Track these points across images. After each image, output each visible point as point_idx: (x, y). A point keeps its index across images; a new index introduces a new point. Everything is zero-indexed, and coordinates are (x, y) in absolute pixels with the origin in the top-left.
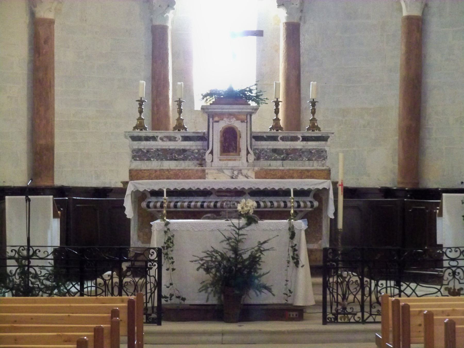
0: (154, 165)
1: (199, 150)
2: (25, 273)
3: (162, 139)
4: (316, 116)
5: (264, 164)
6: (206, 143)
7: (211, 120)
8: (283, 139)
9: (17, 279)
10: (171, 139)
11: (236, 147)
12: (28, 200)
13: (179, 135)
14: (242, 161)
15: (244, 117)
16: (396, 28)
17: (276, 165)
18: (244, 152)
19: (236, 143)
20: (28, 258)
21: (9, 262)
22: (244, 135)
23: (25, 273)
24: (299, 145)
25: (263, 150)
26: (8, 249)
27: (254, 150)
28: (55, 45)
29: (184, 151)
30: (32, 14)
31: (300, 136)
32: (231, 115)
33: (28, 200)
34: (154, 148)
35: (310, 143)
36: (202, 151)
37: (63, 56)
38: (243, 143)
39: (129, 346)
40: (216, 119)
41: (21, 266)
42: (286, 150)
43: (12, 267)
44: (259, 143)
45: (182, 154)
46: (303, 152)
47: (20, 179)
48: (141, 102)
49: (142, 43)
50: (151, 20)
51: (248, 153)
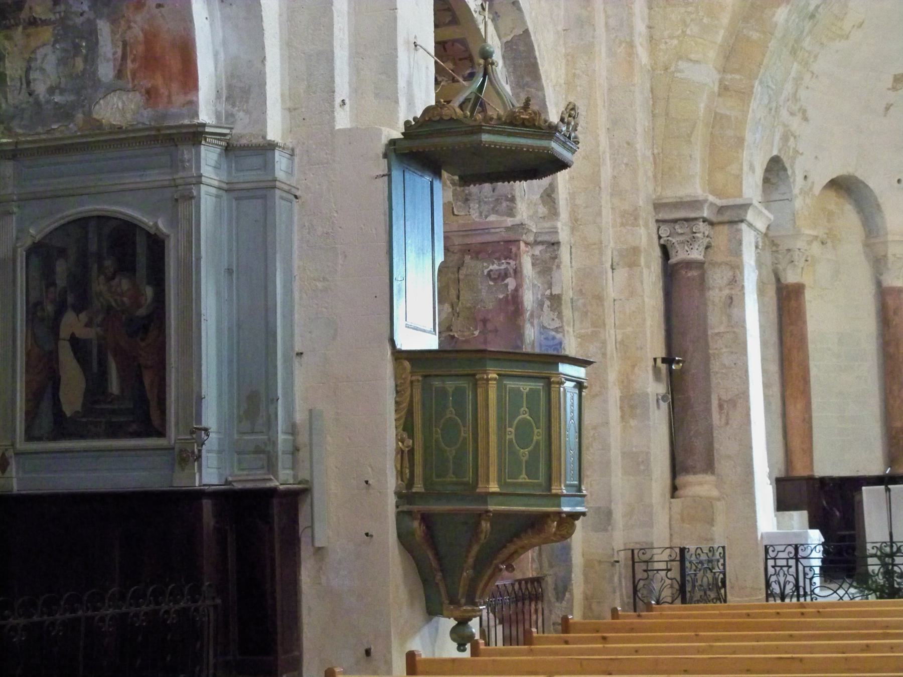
2: (889, 574)
9: (880, 580)
12: (888, 490)
20: (892, 555)
21: (870, 561)
23: (889, 574)
26: (869, 546)
30: (879, 284)
33: (888, 490)
41: (884, 565)
43: (874, 566)
47: (875, 466)
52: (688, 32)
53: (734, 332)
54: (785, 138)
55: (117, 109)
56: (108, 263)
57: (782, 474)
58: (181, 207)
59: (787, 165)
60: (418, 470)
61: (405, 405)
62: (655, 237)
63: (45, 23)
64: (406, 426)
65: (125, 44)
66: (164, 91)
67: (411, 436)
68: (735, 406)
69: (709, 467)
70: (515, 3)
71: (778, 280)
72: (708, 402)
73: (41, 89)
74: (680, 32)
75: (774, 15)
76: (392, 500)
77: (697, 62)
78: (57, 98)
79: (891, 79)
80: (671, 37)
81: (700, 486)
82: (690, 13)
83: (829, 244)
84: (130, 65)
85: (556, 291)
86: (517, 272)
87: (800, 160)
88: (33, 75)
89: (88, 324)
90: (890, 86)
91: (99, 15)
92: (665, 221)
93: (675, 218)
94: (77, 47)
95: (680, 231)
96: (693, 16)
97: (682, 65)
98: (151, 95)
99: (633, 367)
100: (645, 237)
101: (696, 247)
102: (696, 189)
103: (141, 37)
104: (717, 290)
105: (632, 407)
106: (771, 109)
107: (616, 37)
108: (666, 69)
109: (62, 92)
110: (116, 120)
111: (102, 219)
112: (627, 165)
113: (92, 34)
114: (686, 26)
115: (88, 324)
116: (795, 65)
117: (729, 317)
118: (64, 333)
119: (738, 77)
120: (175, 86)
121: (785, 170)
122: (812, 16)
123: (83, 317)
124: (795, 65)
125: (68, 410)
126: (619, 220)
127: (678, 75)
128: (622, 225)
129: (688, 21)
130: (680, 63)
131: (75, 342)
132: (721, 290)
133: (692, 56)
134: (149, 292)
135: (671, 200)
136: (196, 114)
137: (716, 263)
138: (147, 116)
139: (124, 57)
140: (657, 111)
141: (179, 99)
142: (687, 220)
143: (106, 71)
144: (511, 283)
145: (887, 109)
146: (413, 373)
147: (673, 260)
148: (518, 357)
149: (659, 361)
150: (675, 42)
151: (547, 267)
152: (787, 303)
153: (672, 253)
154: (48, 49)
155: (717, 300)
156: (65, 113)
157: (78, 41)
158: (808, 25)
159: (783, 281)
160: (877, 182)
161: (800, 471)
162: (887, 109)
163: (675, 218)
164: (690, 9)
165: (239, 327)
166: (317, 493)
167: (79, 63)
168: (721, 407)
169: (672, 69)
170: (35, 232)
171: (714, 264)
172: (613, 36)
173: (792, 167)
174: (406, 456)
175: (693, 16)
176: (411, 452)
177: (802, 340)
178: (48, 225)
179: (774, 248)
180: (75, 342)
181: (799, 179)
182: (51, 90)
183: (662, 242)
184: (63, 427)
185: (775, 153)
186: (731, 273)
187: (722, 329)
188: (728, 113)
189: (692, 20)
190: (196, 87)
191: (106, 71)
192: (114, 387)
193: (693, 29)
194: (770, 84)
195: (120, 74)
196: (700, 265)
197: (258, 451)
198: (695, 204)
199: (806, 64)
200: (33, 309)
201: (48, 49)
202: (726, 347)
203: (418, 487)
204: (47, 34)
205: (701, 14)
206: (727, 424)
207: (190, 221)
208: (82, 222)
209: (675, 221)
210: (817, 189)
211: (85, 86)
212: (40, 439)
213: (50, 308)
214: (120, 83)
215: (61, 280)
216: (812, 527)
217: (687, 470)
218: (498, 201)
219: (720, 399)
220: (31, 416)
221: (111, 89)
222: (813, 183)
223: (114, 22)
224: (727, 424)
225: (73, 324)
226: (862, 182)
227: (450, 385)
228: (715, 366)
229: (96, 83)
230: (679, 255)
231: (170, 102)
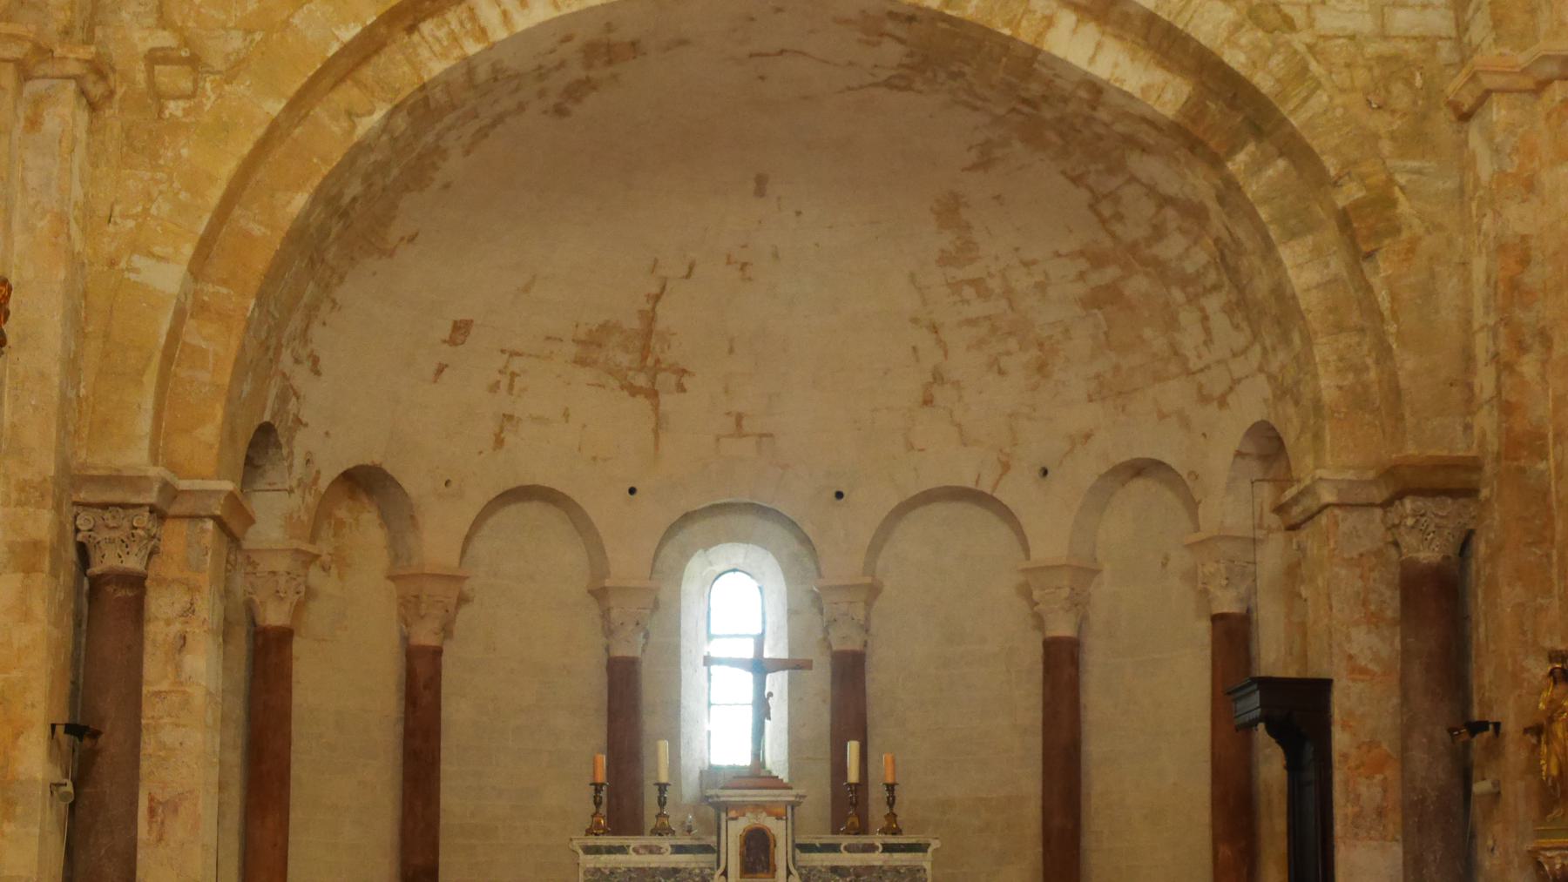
1: (702, 870)
3: (636, 851)
4: (895, 810)
6: (713, 857)
7: (723, 816)
8: (849, 849)
10: (652, 850)
11: (768, 864)
15: (781, 810)
16: (1032, 655)
18: (781, 873)
19: (767, 856)
22: (781, 843)
25: (814, 868)
27: (798, 869)
28: (1337, 713)
29: (676, 871)
31: (878, 843)
32: (758, 807)
34: (623, 867)
35: (896, 856)
36: (707, 871)
37: (457, 712)
38: (781, 856)
39: (1414, 864)
40: (732, 814)
42: (855, 868)
44: (806, 856)
46: (885, 872)
48: (598, 787)
50: (607, 649)
51: (789, 873)
52: (153, 211)
53: (184, 693)
54: (283, 398)
59: (283, 441)
62: (70, 528)
68: (176, 811)
71: (253, 622)
74: (139, 209)
75: (289, 202)
77: (161, 259)
79: (449, 326)
80: (124, 216)
82: (158, 182)
83: (334, 571)
87: (301, 436)
90: (446, 335)
92: (87, 505)
93: (89, 499)
95: (112, 523)
96: (163, 187)
97: (138, 261)
99: (17, 736)
100: (42, 524)
101: (136, 550)
104: (162, 623)
106: (268, 348)
107: (38, 203)
108: (112, 263)
112: (36, 408)
114: (152, 201)
116: (311, 284)
117: (178, 668)
119: (224, 290)
121: (279, 446)
122: (344, 214)
124: (311, 284)
126: (14, 496)
127: (133, 276)
128: (19, 503)
129: (155, 193)
130: (135, 258)
132: (168, 623)
133: (157, 250)
135: (102, 472)
137: (1286, 503)
140: (90, 329)
142: (124, 506)
145: (440, 370)
147: (96, 569)
149: (60, 730)
150: (131, 224)
152: (266, 659)
153: (95, 556)
155: (160, 638)
158: (336, 227)
159: (259, 621)
160: (414, 481)
162: (440, 370)
163: (89, 499)
164: (159, 175)
165: (412, 517)
168: (152, 812)
169: (123, 265)
171: (161, 582)
172: (32, 201)
173: (290, 442)
175: (163, 187)
177: (284, 716)
179: (249, 569)
181: (299, 461)
183: (80, 537)
185: (267, 418)
186: (187, 598)
187: (164, 686)
188: (204, 345)
189: (161, 192)
193: (161, 208)
194: (272, 308)
196: (136, 582)
198: (136, 482)
199: (327, 286)
202: (170, 715)
205: (177, 185)
206: (160, 839)
209: (105, 506)
210: (324, 484)
219: (151, 799)
222: (318, 472)
224: (160, 839)
226: (392, 479)
228: (148, 745)
230: (108, 560)
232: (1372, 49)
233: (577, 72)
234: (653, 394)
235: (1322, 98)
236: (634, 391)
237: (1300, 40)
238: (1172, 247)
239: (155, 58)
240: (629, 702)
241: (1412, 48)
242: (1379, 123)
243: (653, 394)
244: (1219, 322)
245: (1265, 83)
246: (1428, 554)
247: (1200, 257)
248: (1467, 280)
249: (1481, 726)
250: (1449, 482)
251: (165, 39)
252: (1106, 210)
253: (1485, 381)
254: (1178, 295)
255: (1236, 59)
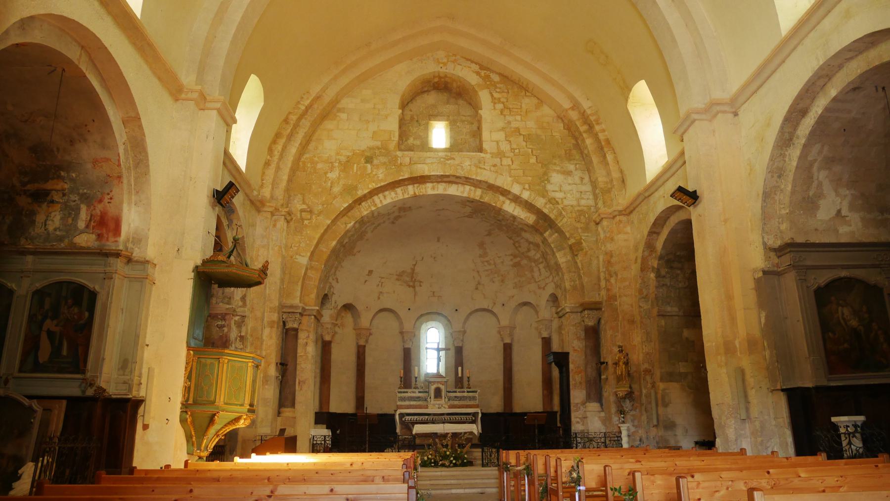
0: (407, 403)
5: (452, 402)
13: (417, 391)
14: (442, 401)
17: (456, 403)
24: (466, 394)
37: (369, 360)
38: (443, 394)
45: (418, 399)
49: (400, 354)
54: (330, 288)
55: (86, 240)
56: (69, 301)
57: (317, 411)
58: (106, 281)
60: (191, 395)
61: (189, 369)
63: (58, 202)
64: (189, 377)
65: (91, 215)
66: (105, 235)
67: (190, 381)
69: (293, 405)
70: (655, 3)
72: (295, 381)
73: (51, 228)
76: (180, 405)
78: (58, 233)
81: (287, 412)
84: (92, 223)
85: (243, 334)
86: (229, 326)
88: (49, 222)
89: (56, 326)
91: (82, 202)
94: (70, 214)
98: (100, 237)
102: (297, 301)
103: (99, 213)
105: (267, 381)
109: (60, 230)
110: (84, 244)
111: (70, 283)
113: (77, 210)
115: (56, 326)
118: (45, 328)
120: (111, 234)
123: (55, 322)
125: (41, 361)
131: (50, 334)
134: (87, 314)
136: (118, 246)
138: (96, 244)
139: (90, 220)
141: (112, 239)
143: (81, 224)
144: (226, 329)
146: (194, 356)
148: (777, 61)
151: (239, 325)
152: (325, 348)
154: (57, 213)
156: (61, 239)
157: (71, 212)
160: (360, 307)
161: (325, 410)
166: (147, 402)
167: (70, 221)
170: (38, 285)
171: (302, 330)
174: (187, 389)
176: (189, 387)
178: (45, 283)
180: (50, 334)
182: (55, 230)
184: (38, 367)
190: (120, 235)
191: (81, 224)
192: (65, 352)
195: (87, 227)
196: (296, 330)
197: (125, 383)
198: (296, 307)
200: (31, 318)
201: (57, 213)
203: (191, 402)
204: (58, 207)
207: (109, 287)
208: (61, 283)
210: (339, 307)
211: (70, 229)
212: (25, 372)
213: (40, 317)
214: (87, 230)
215: (47, 306)
216: (233, 461)
217: (285, 406)
218: (224, 298)
220: (23, 362)
221: (82, 232)
223: (88, 206)
225: (49, 324)
227: (209, 361)
228: (298, 367)
229: (76, 228)
230: (290, 325)
231: (107, 240)
232: (576, 209)
233: (397, 214)
234: (414, 287)
235: (565, 220)
236: (409, 286)
237: (560, 207)
238: (532, 253)
239: (302, 211)
240: (409, 358)
241: (585, 208)
242: (579, 225)
243: (414, 287)
244: (543, 270)
245: (552, 216)
246: (591, 323)
247: (538, 256)
248: (598, 261)
249: (603, 363)
250: (595, 307)
251: (304, 207)
252: (517, 245)
253: (603, 284)
254: (533, 264)
255: (546, 211)
